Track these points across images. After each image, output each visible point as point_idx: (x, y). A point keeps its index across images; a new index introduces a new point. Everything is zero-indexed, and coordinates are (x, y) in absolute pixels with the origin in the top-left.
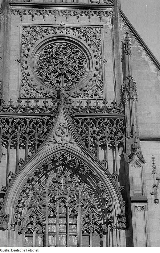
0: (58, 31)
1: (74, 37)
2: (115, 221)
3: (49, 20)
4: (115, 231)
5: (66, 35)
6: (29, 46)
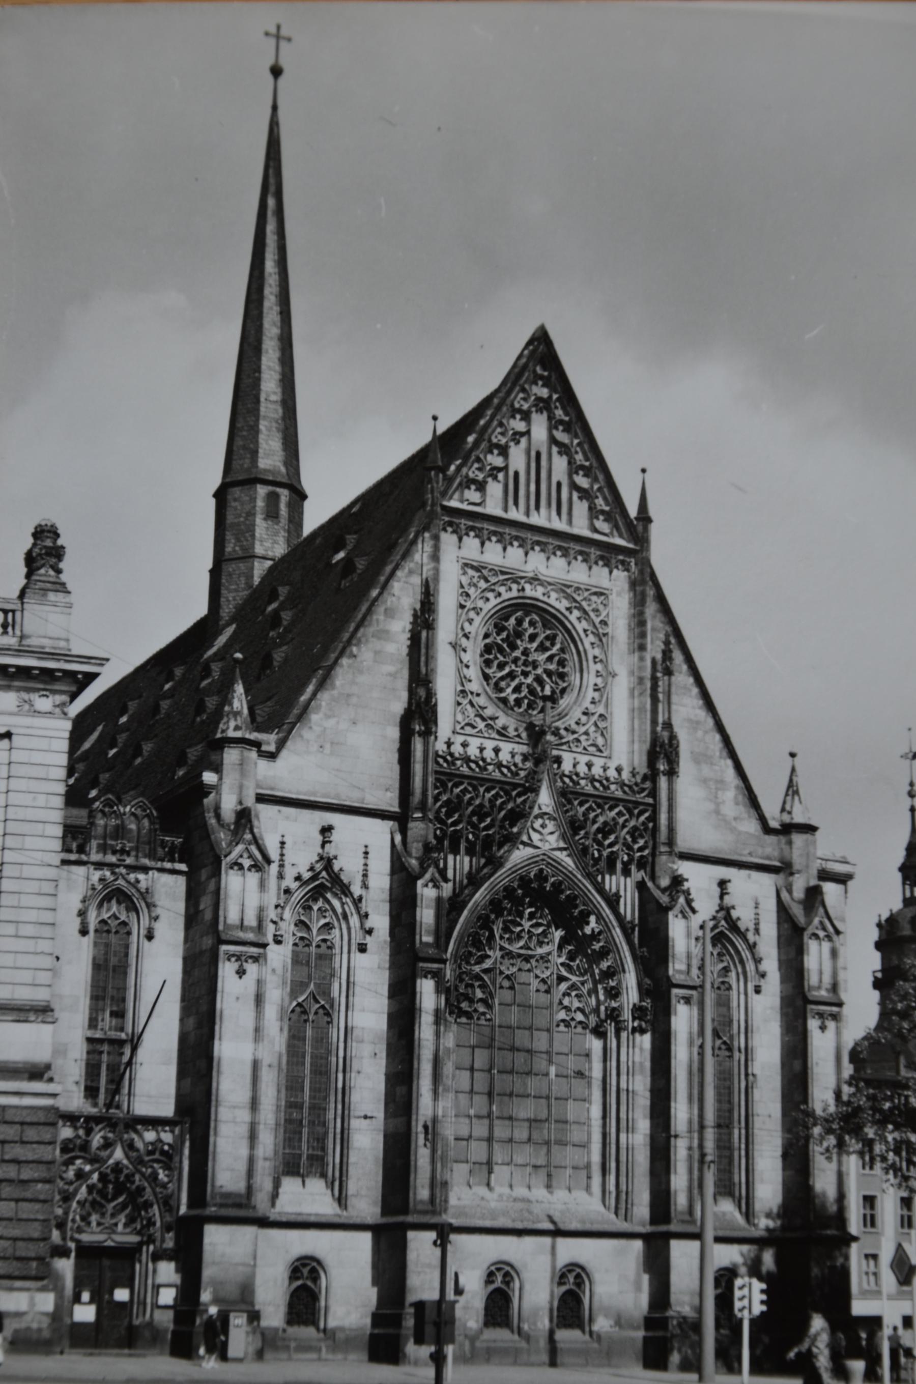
0: (528, 587)
1: (557, 605)
2: (627, 1015)
3: (514, 557)
4: (624, 1035)
5: (541, 598)
6: (472, 614)
